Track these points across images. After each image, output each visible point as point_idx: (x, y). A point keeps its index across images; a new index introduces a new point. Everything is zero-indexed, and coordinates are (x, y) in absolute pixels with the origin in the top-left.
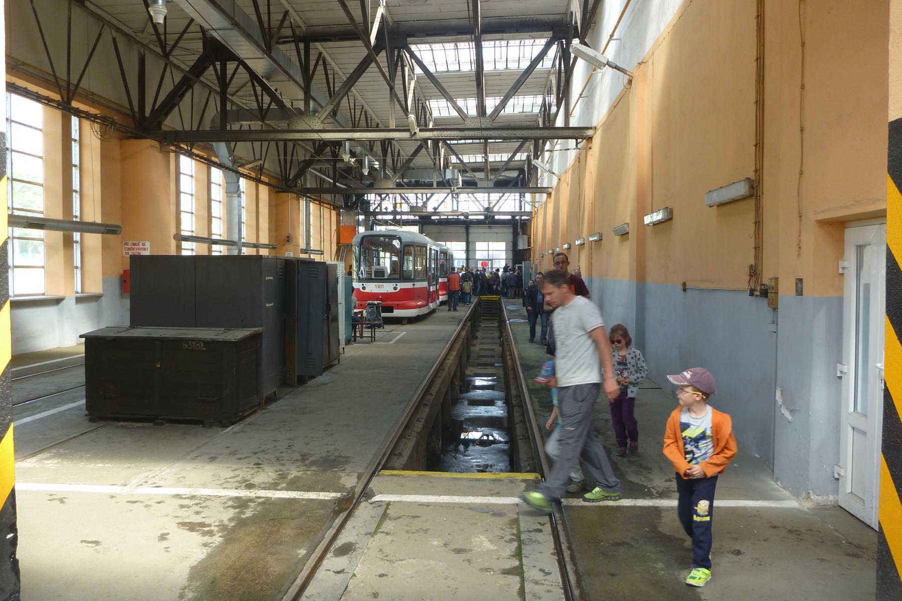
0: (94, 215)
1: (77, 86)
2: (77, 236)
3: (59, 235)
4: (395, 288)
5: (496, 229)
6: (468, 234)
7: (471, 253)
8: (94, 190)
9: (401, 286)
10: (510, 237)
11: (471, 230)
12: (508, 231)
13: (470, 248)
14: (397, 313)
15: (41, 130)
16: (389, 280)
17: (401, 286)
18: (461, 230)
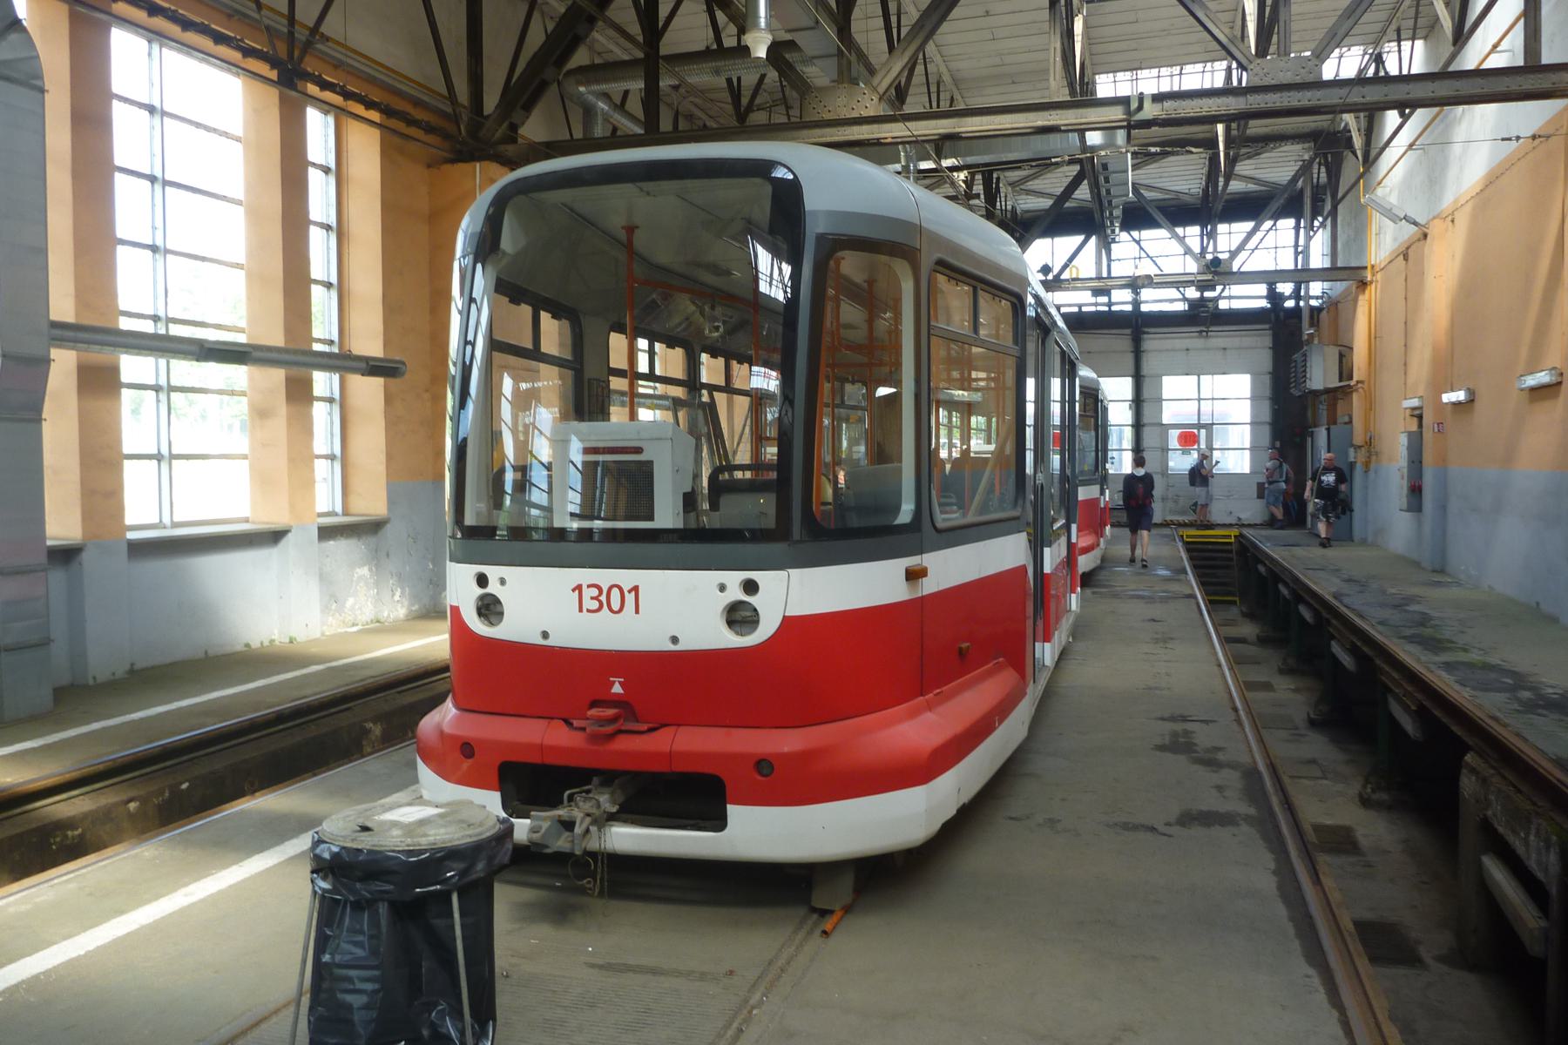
0: (370, 344)
1: (315, 30)
2: (323, 383)
3: (277, 375)
4: (739, 616)
5: (1221, 338)
6: (1138, 353)
7: (1147, 410)
8: (368, 282)
9: (797, 592)
10: (1265, 359)
11: (1151, 343)
12: (1259, 344)
13: (1146, 394)
14: (756, 832)
15: (238, 139)
16: (698, 543)
17: (797, 592)
18: (1120, 342)
